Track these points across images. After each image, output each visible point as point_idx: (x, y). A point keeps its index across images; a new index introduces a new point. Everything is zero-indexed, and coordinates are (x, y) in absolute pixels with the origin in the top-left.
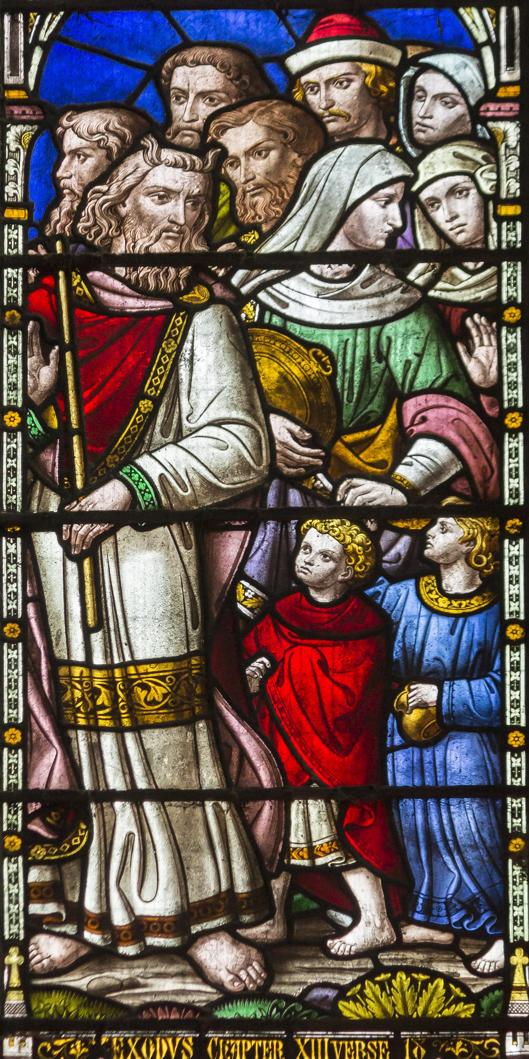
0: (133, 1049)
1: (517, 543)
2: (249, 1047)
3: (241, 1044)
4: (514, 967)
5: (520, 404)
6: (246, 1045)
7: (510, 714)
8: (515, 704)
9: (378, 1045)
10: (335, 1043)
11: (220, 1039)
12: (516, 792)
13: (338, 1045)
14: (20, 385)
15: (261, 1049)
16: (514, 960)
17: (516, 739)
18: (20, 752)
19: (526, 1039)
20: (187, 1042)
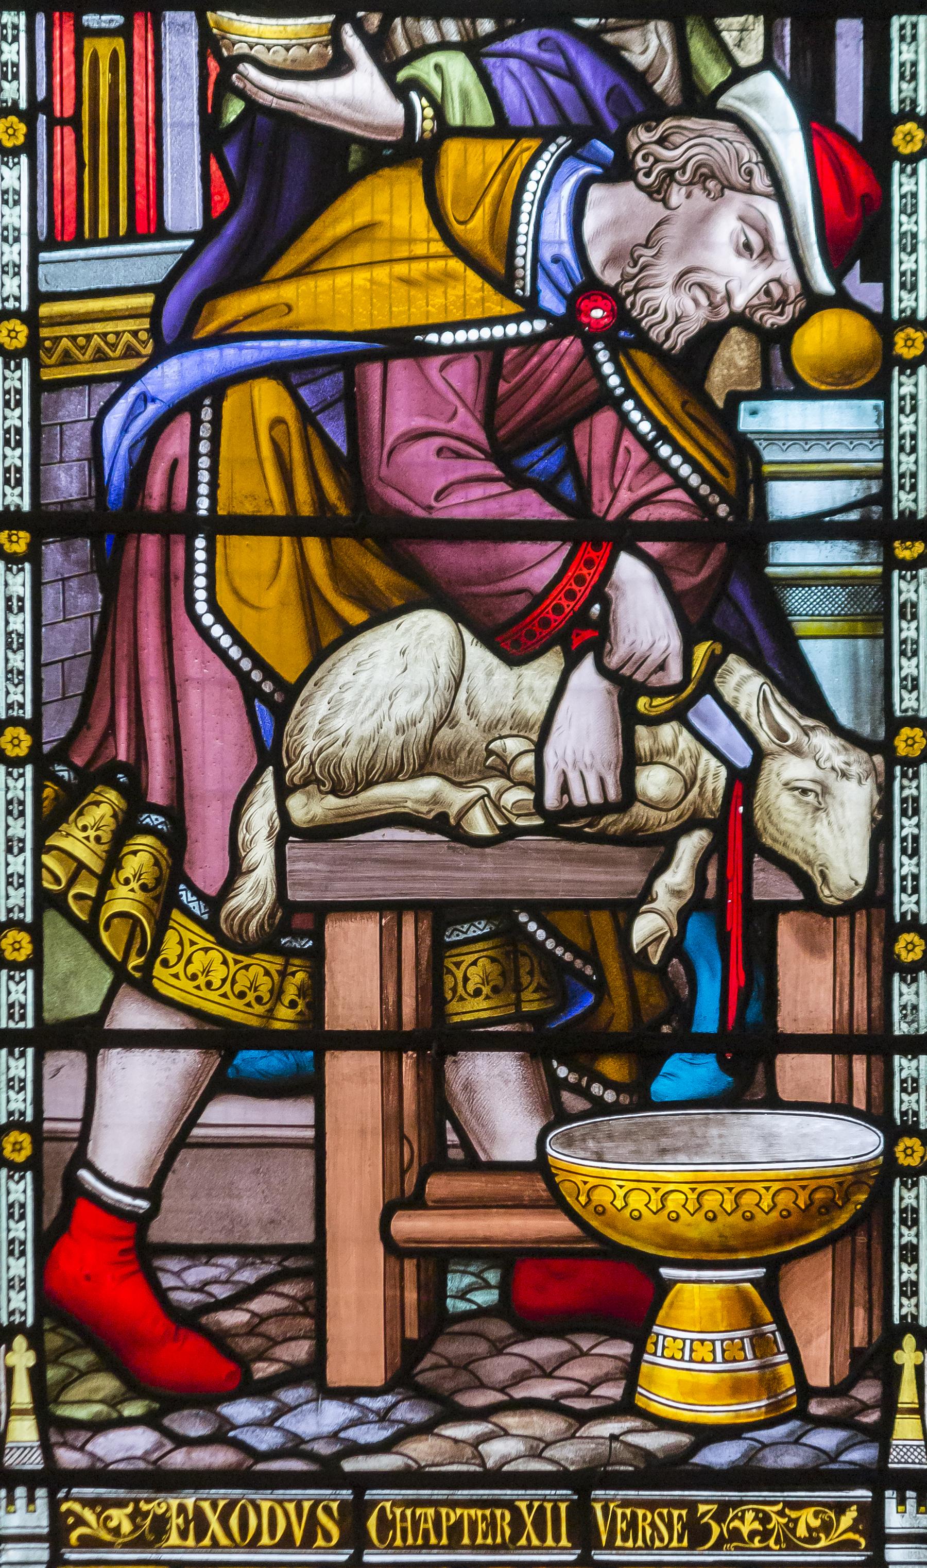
2: (453, 1520)
5: (897, 166)
6: (448, 1515)
9: (670, 1515)
11: (395, 1504)
14: (25, 230)
15: (473, 1524)
18: (25, 362)
19: (919, 1504)
20: (328, 1510)
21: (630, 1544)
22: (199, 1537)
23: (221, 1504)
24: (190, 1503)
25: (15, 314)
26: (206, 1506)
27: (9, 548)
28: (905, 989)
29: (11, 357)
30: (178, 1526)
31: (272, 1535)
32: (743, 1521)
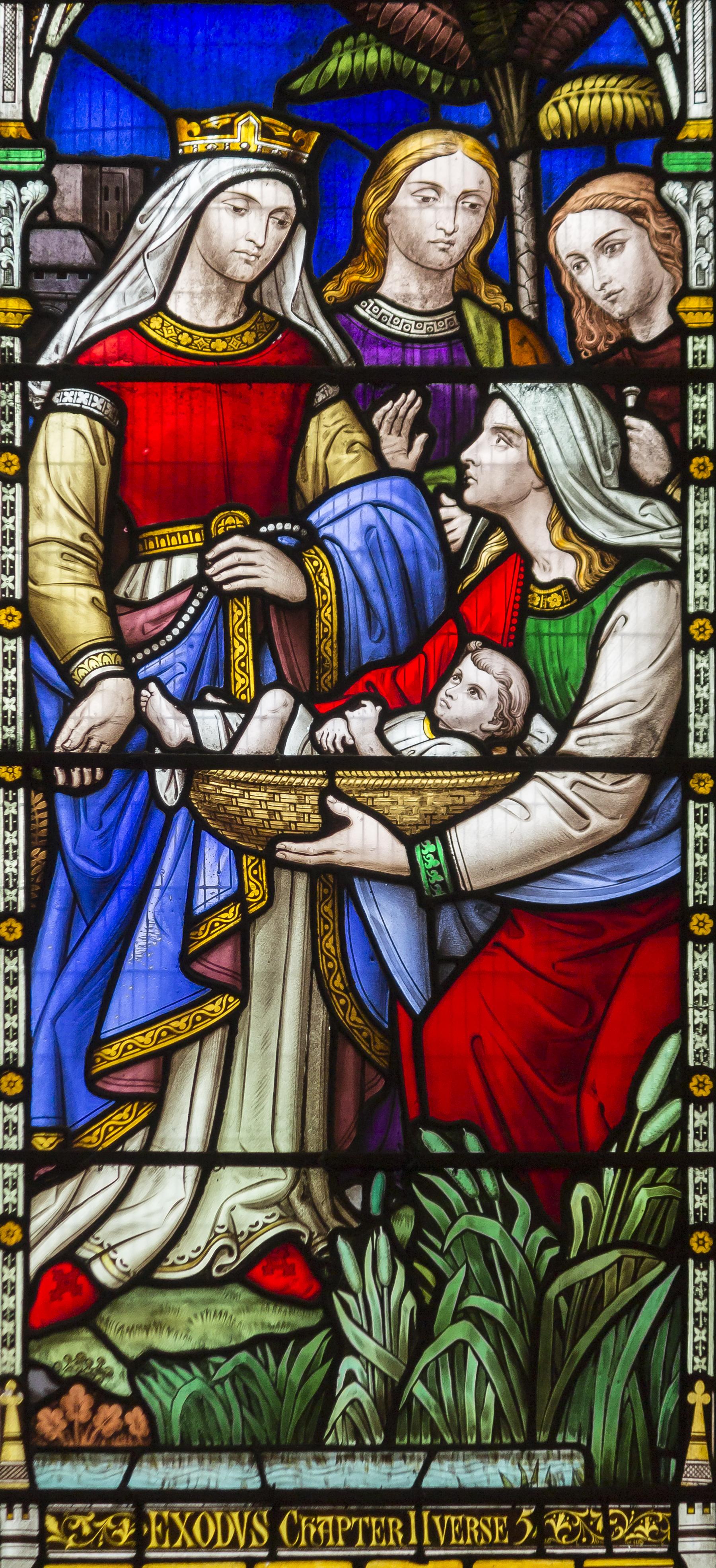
0: (183, 1531)
1: (706, 653)
3: (335, 1522)
4: (693, 1406)
7: (695, 1202)
8: (701, 874)
9: (493, 1522)
10: (437, 1519)
12: (701, 1160)
13: (442, 1521)
16: (691, 1398)
17: (701, 924)
21: (462, 1541)
22: (173, 1540)
23: (188, 1515)
24: (165, 1514)
25: (11, 602)
26: (176, 1516)
27: (9, 778)
28: (697, 1114)
29: (10, 948)
30: (157, 1533)
31: (225, 1539)
32: (644, 1525)
